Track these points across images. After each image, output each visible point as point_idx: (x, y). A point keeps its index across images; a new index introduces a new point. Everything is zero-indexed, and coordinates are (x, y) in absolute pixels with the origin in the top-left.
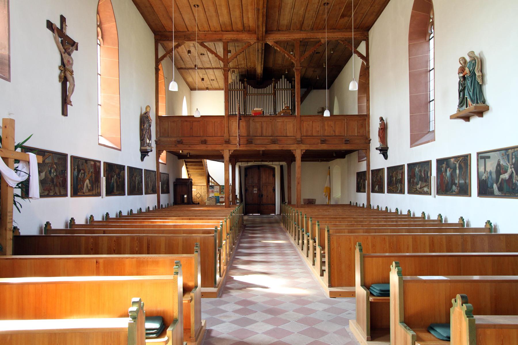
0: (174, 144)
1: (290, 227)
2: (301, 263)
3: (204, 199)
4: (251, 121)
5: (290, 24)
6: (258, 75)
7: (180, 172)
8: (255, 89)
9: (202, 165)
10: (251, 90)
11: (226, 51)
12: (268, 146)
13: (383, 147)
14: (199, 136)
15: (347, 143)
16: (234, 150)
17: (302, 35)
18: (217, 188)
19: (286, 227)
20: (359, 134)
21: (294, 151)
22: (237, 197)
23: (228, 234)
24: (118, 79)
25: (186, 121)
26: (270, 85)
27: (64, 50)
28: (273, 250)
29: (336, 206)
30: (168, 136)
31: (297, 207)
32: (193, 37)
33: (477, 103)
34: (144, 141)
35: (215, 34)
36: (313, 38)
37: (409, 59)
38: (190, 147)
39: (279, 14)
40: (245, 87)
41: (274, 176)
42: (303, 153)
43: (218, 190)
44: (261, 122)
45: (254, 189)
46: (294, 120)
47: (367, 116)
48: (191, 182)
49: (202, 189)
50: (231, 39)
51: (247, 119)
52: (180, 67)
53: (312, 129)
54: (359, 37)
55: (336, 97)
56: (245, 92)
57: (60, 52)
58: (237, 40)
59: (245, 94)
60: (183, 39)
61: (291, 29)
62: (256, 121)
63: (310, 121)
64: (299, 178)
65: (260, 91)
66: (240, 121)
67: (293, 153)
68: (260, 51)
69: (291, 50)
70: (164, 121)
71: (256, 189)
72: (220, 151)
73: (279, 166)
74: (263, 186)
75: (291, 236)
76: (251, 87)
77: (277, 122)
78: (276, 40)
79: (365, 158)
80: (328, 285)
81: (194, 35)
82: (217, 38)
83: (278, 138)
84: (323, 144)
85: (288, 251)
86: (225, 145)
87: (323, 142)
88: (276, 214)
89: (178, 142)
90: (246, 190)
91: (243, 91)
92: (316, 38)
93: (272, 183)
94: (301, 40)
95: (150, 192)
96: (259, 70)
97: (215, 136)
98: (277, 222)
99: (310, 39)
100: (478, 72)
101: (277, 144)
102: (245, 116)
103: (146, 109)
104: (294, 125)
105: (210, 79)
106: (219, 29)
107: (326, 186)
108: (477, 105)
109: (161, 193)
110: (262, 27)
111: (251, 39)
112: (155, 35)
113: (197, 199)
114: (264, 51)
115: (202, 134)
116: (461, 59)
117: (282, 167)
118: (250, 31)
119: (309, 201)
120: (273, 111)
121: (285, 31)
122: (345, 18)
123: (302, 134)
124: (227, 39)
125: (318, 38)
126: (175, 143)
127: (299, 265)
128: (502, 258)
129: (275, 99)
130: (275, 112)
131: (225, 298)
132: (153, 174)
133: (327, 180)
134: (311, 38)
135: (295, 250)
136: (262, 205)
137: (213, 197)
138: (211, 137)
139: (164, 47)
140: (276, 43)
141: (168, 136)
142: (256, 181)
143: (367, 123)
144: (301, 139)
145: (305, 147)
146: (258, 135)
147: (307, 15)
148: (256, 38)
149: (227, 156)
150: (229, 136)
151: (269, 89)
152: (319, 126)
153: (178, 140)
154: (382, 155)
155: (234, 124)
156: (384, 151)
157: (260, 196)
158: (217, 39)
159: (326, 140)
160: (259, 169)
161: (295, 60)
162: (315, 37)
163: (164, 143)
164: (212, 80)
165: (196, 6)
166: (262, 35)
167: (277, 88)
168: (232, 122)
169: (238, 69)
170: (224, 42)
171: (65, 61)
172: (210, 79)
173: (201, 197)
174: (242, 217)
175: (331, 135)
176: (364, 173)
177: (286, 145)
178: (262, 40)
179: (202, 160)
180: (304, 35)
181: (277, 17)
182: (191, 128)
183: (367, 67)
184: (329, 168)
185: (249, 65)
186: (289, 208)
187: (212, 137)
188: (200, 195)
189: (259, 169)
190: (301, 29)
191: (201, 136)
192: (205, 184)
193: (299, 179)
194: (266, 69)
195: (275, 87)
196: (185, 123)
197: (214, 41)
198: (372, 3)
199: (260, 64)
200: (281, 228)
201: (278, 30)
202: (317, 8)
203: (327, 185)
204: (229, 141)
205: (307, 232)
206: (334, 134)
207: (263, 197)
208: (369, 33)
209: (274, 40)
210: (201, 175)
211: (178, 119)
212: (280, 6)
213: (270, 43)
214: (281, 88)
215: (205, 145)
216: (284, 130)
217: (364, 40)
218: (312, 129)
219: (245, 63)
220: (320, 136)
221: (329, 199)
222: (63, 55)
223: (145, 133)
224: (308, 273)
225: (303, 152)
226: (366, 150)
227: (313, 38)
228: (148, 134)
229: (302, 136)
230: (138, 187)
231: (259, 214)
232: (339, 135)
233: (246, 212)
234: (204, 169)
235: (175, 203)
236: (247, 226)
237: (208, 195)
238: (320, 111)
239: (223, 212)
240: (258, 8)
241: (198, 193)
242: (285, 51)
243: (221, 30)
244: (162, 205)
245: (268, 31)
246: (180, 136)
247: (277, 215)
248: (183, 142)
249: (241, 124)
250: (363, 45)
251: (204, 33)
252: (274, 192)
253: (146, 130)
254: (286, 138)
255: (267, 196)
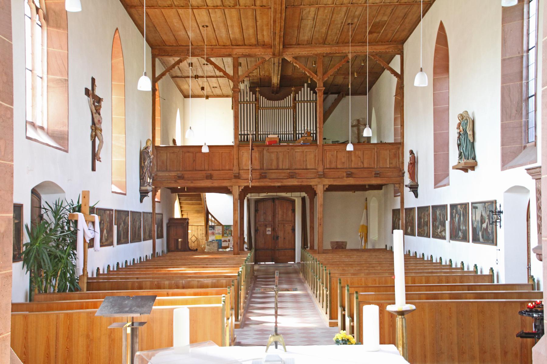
0: (174, 179)
1: (308, 277)
2: (314, 308)
3: (201, 243)
4: (265, 151)
5: (311, 39)
6: (274, 84)
7: (171, 210)
8: (270, 101)
9: (201, 200)
10: (264, 102)
11: (236, 65)
12: (285, 180)
13: (413, 184)
14: (204, 169)
15: (377, 177)
16: (245, 186)
17: (325, 49)
18: (219, 229)
19: (305, 277)
20: (391, 166)
21: (315, 187)
22: (244, 239)
23: (244, 281)
24: (124, 117)
25: (188, 152)
26: (289, 96)
27: (95, 111)
28: (288, 299)
29: (374, 250)
30: (167, 170)
31: (318, 253)
32: (198, 52)
33: (468, 159)
34: (145, 180)
35: (224, 48)
36: (338, 53)
37: (434, 94)
38: (192, 182)
39: (298, 32)
40: (257, 99)
41: (294, 211)
42: (325, 189)
43: (220, 231)
44: (277, 152)
45: (267, 229)
46: (315, 150)
47: (401, 144)
48: (188, 223)
49: (199, 230)
50: (242, 54)
51: (261, 149)
52: (174, 75)
53: (337, 160)
54: (392, 51)
55: (373, 108)
56: (257, 105)
57: (92, 112)
58: (249, 56)
59: (257, 108)
60: (185, 54)
61: (313, 43)
62: (271, 151)
63: (334, 151)
64: (321, 218)
65: (276, 103)
66: (252, 151)
67: (314, 189)
68: (277, 64)
69: (313, 62)
70: (162, 152)
71: (270, 229)
72: (228, 187)
73: (300, 198)
74: (279, 225)
75: (309, 286)
76: (265, 98)
77: (296, 152)
78: (295, 55)
79: (399, 194)
80: (329, 318)
81: (199, 50)
82: (226, 53)
83: (296, 171)
84: (349, 178)
85: (303, 299)
86: (234, 180)
87: (349, 175)
88: (296, 262)
89: (179, 177)
90: (256, 231)
91: (254, 104)
92: (342, 53)
93: (291, 221)
94: (325, 55)
95: (147, 238)
96: (275, 80)
97: (222, 170)
98: (296, 272)
99: (334, 53)
100: (470, 130)
101: (295, 179)
102: (249, 77)
103: (147, 143)
104: (315, 156)
105: (212, 86)
106: (228, 43)
107: (362, 223)
108: (468, 161)
109: (157, 238)
110: (278, 46)
111: (266, 54)
112: (152, 49)
113: (192, 243)
114: (281, 64)
115: (206, 168)
116: (459, 116)
117: (303, 199)
118: (264, 45)
119: (337, 244)
120: (292, 130)
121: (306, 45)
122: (373, 34)
123: (324, 166)
124: (238, 54)
125: (345, 53)
126: (174, 178)
127: (311, 309)
128: (432, 287)
129: (295, 122)
130: (295, 131)
131: (245, 329)
132: (150, 215)
133: (363, 217)
134: (336, 53)
135: (310, 299)
136: (277, 250)
137: (214, 241)
138: (217, 170)
139: (163, 63)
140: (296, 58)
141: (166, 170)
142: (270, 218)
143: (400, 152)
144: (323, 171)
145: (327, 182)
146: (274, 168)
147: (329, 32)
148: (271, 54)
149: (236, 191)
150: (239, 170)
151: (288, 101)
152: (344, 157)
153: (180, 175)
154: (412, 193)
155: (246, 155)
156: (414, 189)
157: (276, 238)
158: (226, 55)
159: (353, 173)
160: (274, 202)
161: (317, 79)
162: (341, 52)
163: (161, 179)
164: (214, 87)
165: (205, 26)
166: (278, 52)
167: (297, 100)
168: (243, 152)
169: (248, 78)
170: (234, 58)
171: (96, 121)
172: (212, 86)
173: (197, 242)
174: (253, 266)
175: (359, 167)
176: (398, 210)
177: (305, 180)
178: (279, 55)
179: (201, 194)
180: (328, 49)
181: (296, 34)
182: (194, 161)
183: (401, 87)
184: (366, 200)
185: (262, 73)
186: (308, 255)
187: (219, 170)
188: (195, 239)
189: (274, 202)
190: (324, 42)
191: (206, 169)
192: (203, 223)
193: (320, 220)
194: (283, 78)
195: (295, 99)
196: (187, 154)
197: (223, 57)
198: (401, 23)
199: (276, 75)
200: (300, 279)
201: (298, 44)
202: (341, 27)
203: (363, 222)
204: (238, 176)
205: (319, 279)
206: (362, 166)
207: (278, 239)
208: (404, 46)
209: (293, 56)
210: (198, 212)
211: (179, 150)
212: (299, 26)
213: (289, 59)
214: (302, 100)
215: (210, 180)
216: (304, 161)
217: (398, 54)
218: (337, 160)
219: (258, 72)
220: (346, 168)
221: (366, 241)
222: (94, 115)
223: (146, 171)
224: (318, 314)
225: (325, 188)
226: (400, 184)
227: (338, 53)
228: (149, 172)
229: (325, 169)
230: (138, 234)
231: (274, 263)
232: (368, 167)
233: (257, 261)
234: (202, 205)
235: (169, 250)
236: (258, 277)
237: (207, 239)
238: (354, 124)
239: (225, 262)
240: (274, 32)
241: (194, 235)
242: (305, 67)
243: (231, 44)
244: (157, 253)
245: (286, 45)
246: (181, 169)
247: (298, 263)
248: (184, 177)
249: (254, 154)
250: (398, 58)
251: (211, 47)
252: (293, 232)
253: (147, 167)
254: (306, 171)
255: (284, 238)
